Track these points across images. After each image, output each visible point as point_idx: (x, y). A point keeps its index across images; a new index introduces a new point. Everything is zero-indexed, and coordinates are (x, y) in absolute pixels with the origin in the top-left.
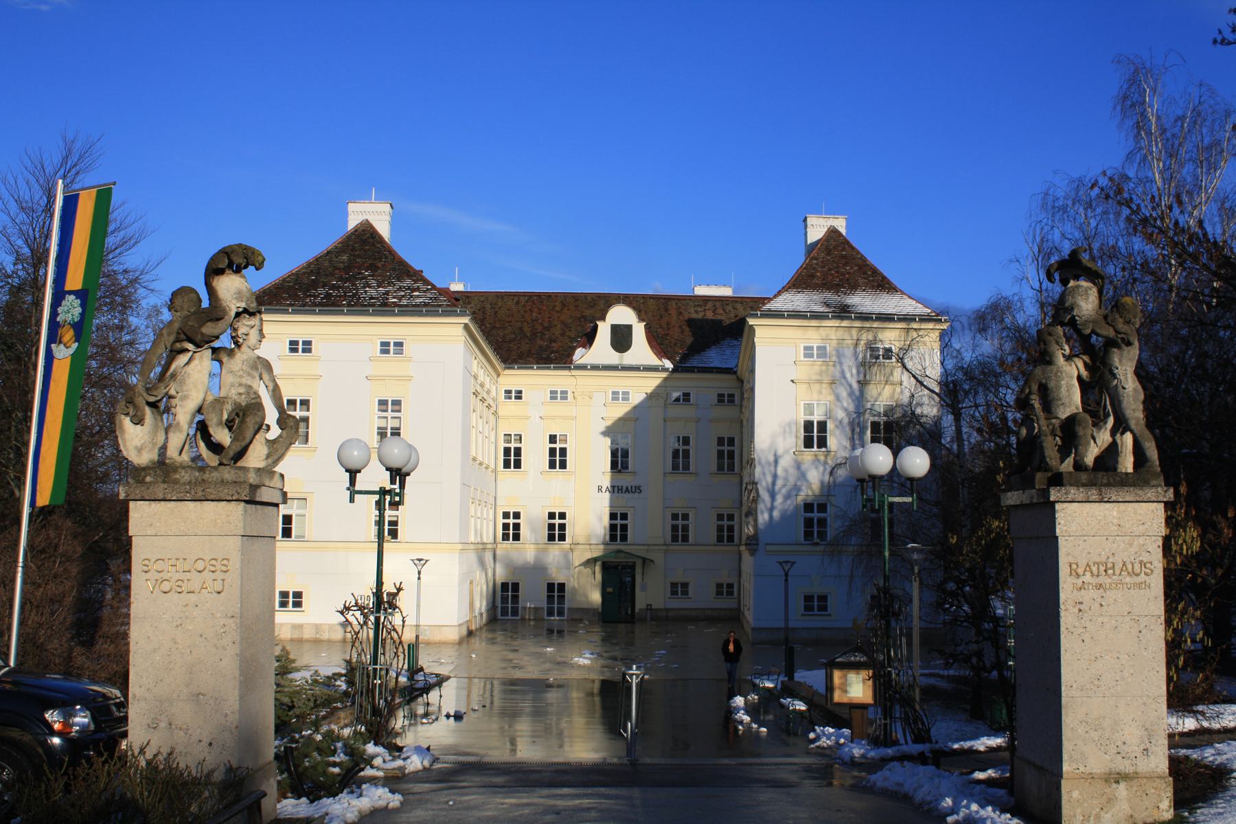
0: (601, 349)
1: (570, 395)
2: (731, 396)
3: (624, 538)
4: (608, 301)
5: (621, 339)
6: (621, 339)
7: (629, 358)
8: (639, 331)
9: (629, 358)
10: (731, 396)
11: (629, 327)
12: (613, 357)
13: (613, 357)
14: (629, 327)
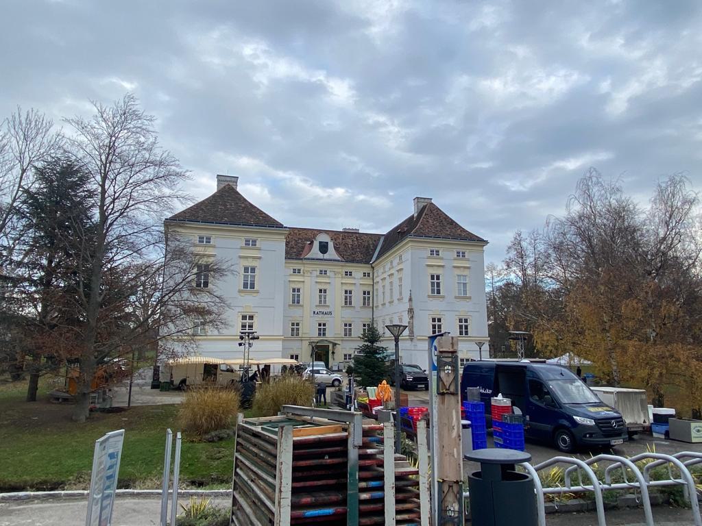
0: (315, 252)
1: (301, 271)
2: (369, 274)
3: (324, 334)
4: (320, 231)
5: (324, 248)
6: (324, 248)
7: (326, 256)
8: (331, 245)
9: (326, 256)
10: (369, 274)
11: (327, 243)
12: (321, 256)
13: (321, 256)
14: (327, 243)
